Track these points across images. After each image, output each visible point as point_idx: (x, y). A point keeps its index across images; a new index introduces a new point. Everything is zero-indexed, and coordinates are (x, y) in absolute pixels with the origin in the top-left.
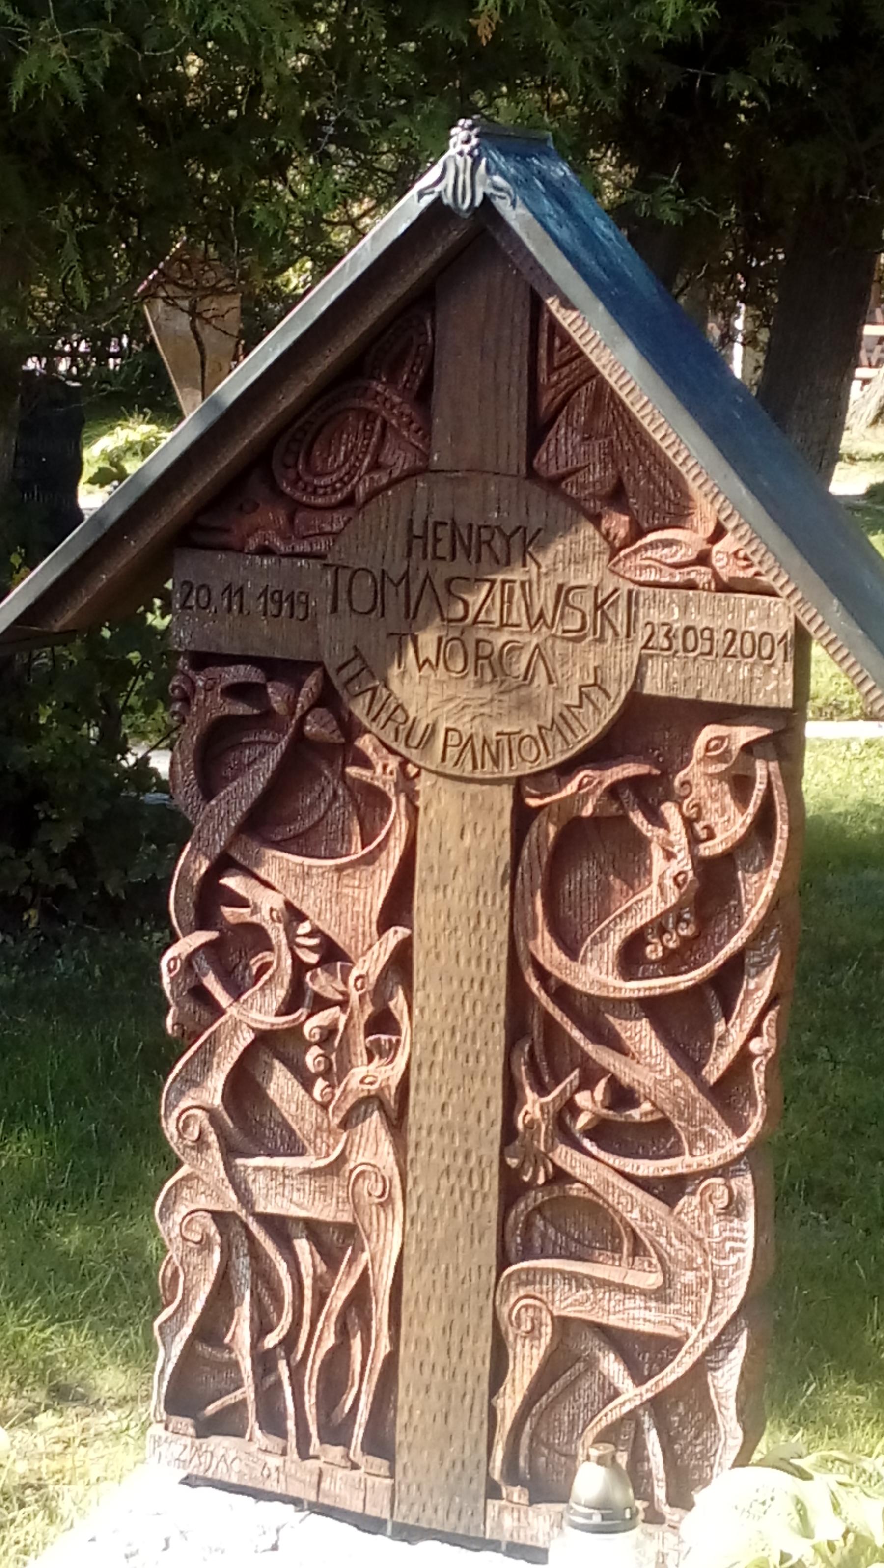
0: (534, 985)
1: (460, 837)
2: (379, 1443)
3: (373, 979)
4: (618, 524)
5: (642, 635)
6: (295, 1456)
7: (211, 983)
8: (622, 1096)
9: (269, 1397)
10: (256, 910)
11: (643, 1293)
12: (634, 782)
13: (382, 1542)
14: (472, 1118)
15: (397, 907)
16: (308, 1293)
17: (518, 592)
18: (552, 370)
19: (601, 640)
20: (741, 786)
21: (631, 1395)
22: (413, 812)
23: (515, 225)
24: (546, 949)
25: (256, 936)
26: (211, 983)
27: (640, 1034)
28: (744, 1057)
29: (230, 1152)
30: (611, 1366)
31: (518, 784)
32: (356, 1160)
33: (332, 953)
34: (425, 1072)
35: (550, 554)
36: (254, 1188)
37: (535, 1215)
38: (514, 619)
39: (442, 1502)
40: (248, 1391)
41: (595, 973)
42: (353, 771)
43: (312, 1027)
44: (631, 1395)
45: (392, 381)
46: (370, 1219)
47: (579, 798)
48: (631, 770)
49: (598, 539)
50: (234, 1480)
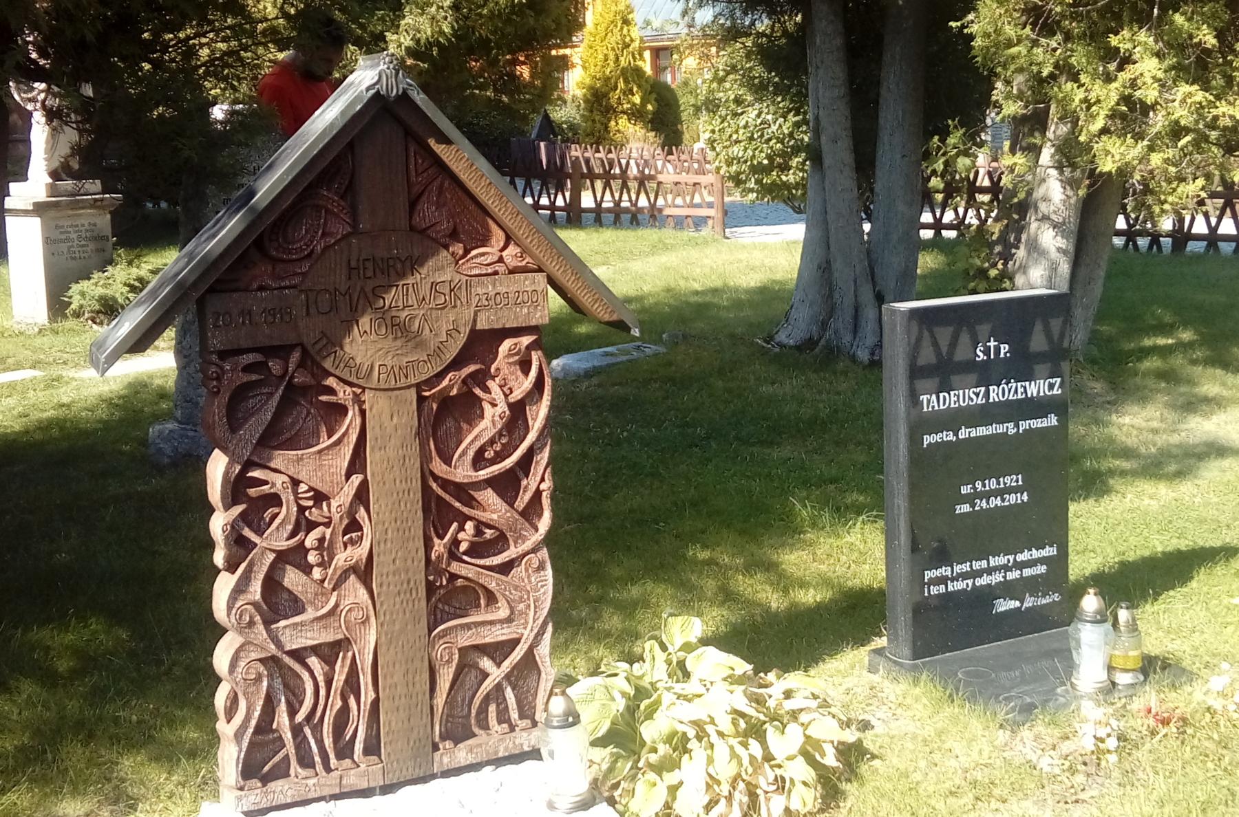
0: (434, 486)
1: (390, 420)
3: (347, 505)
4: (458, 248)
5: (474, 301)
6: (324, 774)
7: (247, 532)
8: (480, 526)
10: (274, 485)
11: (501, 621)
12: (470, 375)
13: (377, 800)
14: (409, 562)
15: (357, 462)
16: (322, 684)
17: (411, 290)
18: (417, 175)
19: (455, 306)
22: (363, 413)
23: (419, 103)
24: (438, 467)
25: (275, 500)
26: (247, 532)
27: (489, 496)
28: (538, 493)
29: (267, 623)
30: (486, 663)
31: (419, 387)
32: (346, 603)
33: (320, 497)
34: (382, 545)
35: (426, 268)
36: (282, 639)
37: (447, 598)
38: (410, 303)
39: (410, 764)
41: (463, 472)
42: (323, 398)
45: (328, 190)
47: (450, 387)
48: (472, 368)
49: (449, 257)
50: (289, 801)
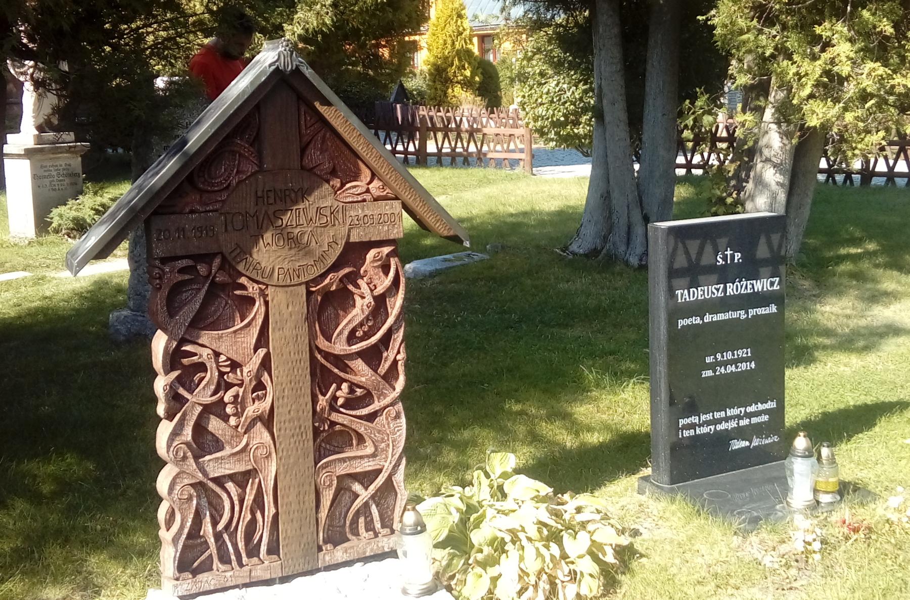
0: (319, 357)
1: (286, 308)
3: (255, 371)
4: (337, 182)
5: (348, 221)
6: (238, 568)
7: (182, 391)
8: (353, 386)
10: (201, 356)
11: (368, 456)
12: (346, 276)
13: (277, 587)
14: (301, 412)
15: (262, 340)
16: (236, 502)
17: (302, 213)
18: (306, 129)
19: (334, 225)
22: (266, 303)
23: (308, 75)
24: (322, 343)
25: (202, 367)
26: (182, 391)
27: (359, 365)
28: (395, 362)
29: (196, 458)
30: (357, 487)
31: (307, 284)
32: (254, 443)
33: (235, 365)
34: (281, 400)
35: (313, 197)
36: (207, 469)
38: (301, 222)
39: (301, 561)
41: (340, 347)
42: (238, 292)
45: (241, 139)
47: (331, 284)
48: (347, 270)
49: (330, 189)
50: (212, 588)
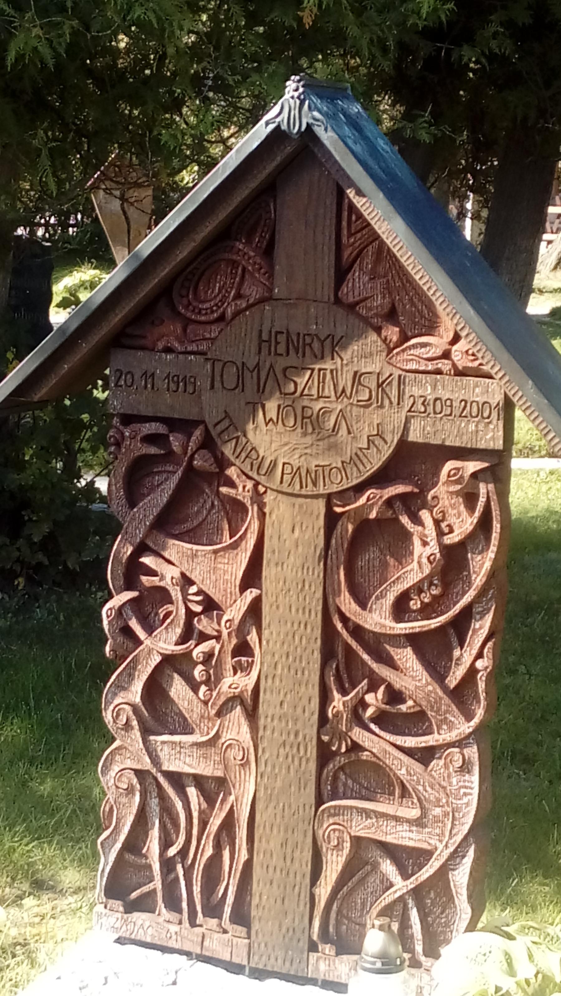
0: (339, 626)
1: (292, 532)
2: (241, 917)
3: (236, 622)
4: (392, 333)
5: (407, 403)
6: (187, 925)
7: (134, 624)
8: (395, 696)
9: (170, 887)
10: (162, 578)
11: (408, 821)
12: (402, 497)
13: (242, 980)
14: (299, 710)
15: (252, 576)
16: (195, 821)
17: (328, 376)
18: (350, 235)
19: (382, 406)
20: (470, 499)
21: (401, 886)
22: (262, 516)
23: (327, 143)
24: (347, 603)
25: (163, 595)
26: (134, 624)
27: (406, 657)
28: (472, 671)
29: (146, 732)
30: (388, 868)
31: (329, 498)
32: (226, 737)
33: (210, 606)
34: (270, 681)
35: (349, 352)
36: (161, 755)
37: (340, 772)
38: (326, 393)
39: (280, 954)
40: (157, 884)
41: (378, 618)
42: (224, 490)
43: (198, 652)
44: (401, 886)
45: (249, 242)
46: (235, 775)
47: (367, 507)
48: (400, 489)
49: (380, 343)
50: (149, 940)
